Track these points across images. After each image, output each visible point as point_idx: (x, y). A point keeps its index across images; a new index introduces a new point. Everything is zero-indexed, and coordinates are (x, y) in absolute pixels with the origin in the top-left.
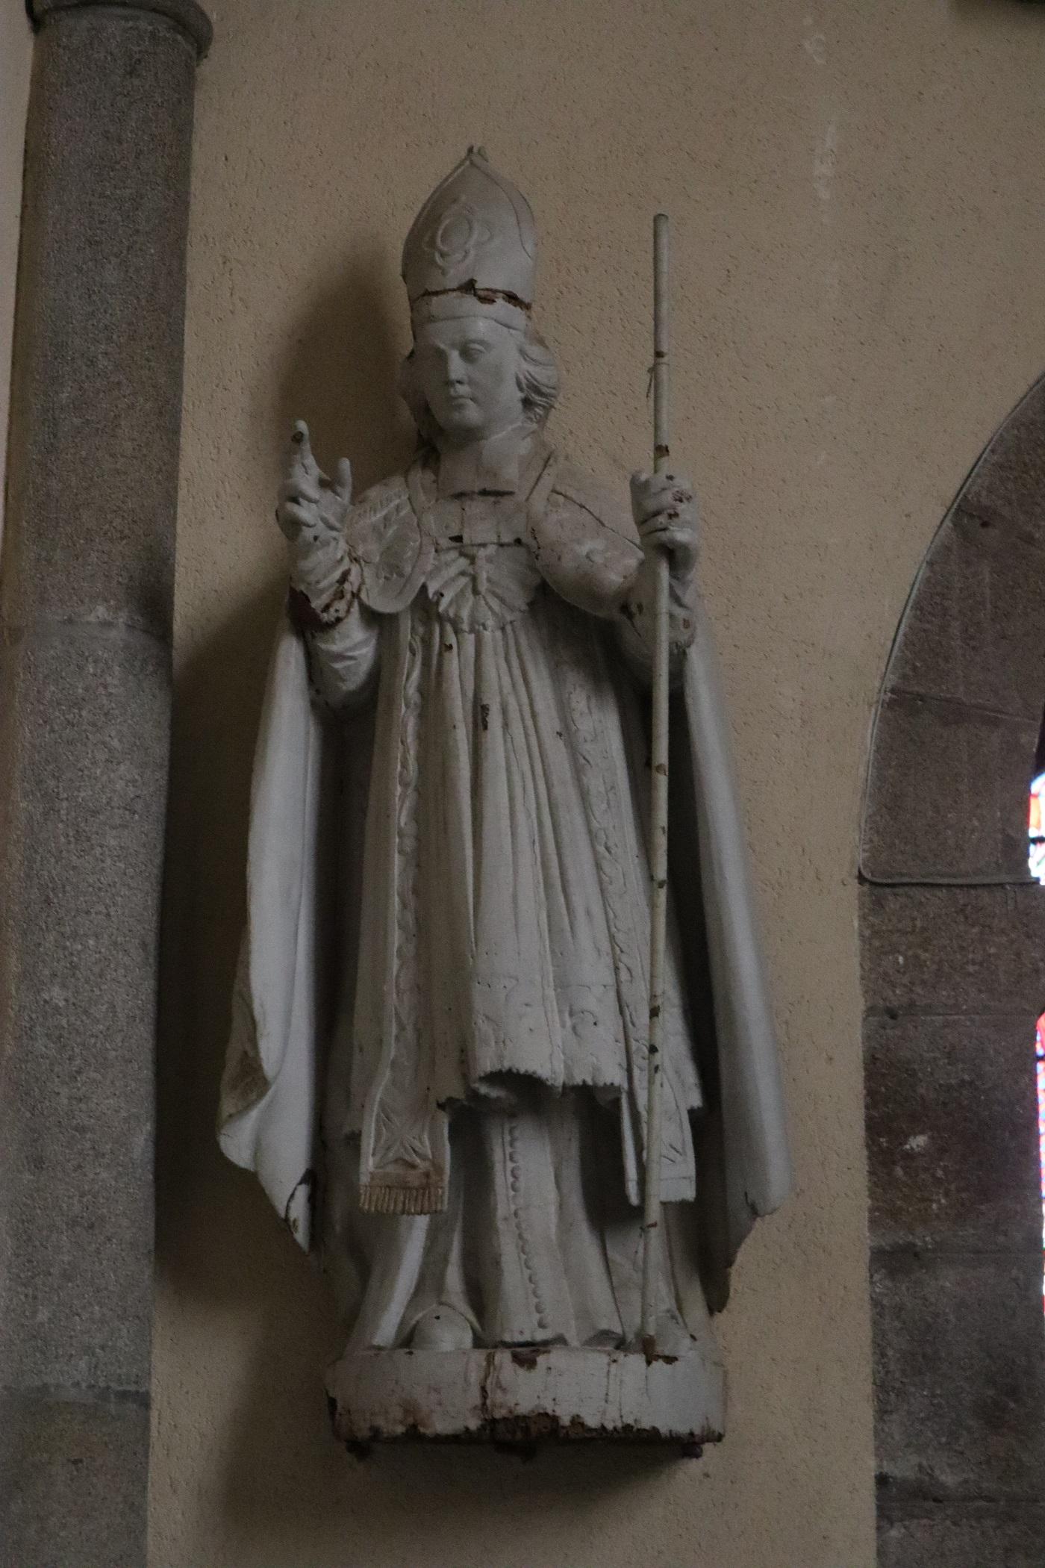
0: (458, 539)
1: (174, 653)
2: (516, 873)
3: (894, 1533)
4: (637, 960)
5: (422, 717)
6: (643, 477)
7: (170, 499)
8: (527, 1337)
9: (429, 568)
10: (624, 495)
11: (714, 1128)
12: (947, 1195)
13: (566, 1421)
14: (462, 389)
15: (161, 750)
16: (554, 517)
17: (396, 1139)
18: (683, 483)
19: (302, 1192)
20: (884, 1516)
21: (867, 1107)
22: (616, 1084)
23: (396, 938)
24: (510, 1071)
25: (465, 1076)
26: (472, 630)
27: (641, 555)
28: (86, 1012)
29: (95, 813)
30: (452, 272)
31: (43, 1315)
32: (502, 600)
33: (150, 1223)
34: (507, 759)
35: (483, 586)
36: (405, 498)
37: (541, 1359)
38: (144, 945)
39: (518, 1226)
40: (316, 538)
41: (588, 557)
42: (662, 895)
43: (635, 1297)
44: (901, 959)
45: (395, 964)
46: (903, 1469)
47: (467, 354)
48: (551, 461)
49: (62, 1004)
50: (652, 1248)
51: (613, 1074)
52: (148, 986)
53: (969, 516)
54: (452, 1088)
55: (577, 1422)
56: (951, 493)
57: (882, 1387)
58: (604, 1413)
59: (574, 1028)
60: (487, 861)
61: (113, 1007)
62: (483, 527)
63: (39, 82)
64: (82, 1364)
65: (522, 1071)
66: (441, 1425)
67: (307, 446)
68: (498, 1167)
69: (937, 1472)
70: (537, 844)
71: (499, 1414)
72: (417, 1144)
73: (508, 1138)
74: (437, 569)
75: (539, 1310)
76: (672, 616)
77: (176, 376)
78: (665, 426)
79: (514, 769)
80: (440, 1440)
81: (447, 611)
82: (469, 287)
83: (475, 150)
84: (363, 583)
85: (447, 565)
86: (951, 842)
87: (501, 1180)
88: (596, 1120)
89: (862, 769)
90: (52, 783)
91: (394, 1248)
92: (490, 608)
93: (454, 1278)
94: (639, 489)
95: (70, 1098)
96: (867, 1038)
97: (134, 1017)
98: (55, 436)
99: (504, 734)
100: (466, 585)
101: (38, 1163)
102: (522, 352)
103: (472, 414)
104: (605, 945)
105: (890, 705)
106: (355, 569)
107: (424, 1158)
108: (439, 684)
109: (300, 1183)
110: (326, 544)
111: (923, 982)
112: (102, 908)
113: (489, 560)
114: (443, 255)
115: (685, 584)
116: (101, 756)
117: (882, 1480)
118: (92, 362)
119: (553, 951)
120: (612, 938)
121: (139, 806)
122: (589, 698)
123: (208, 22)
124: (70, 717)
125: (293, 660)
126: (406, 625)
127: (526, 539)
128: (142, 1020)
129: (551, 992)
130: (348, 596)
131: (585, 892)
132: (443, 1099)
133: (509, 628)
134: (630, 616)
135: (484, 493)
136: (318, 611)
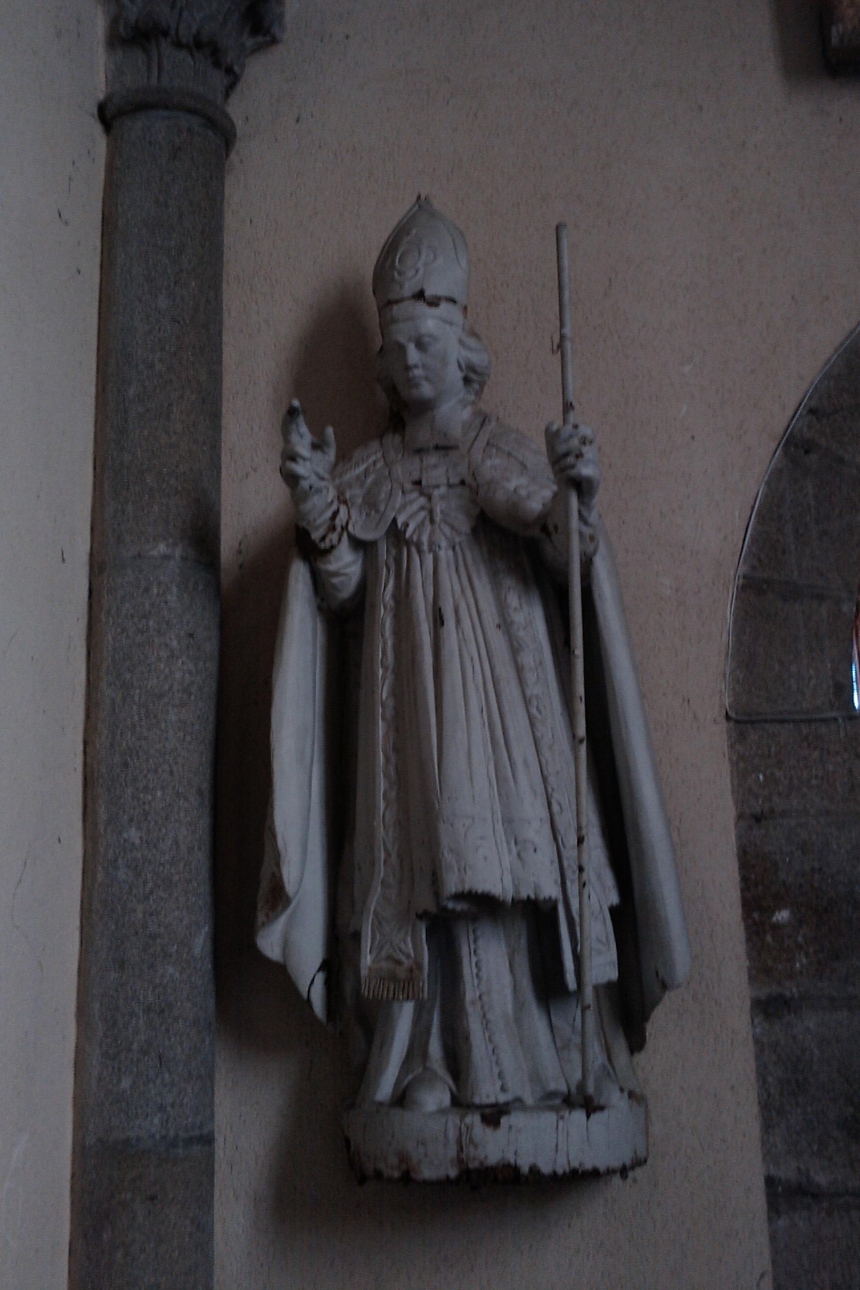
0: (418, 483)
1: (222, 575)
2: (469, 733)
3: (783, 1222)
4: (563, 796)
5: (396, 617)
6: (555, 427)
7: (215, 465)
8: (492, 1100)
9: (397, 506)
10: (541, 443)
11: (631, 920)
12: (807, 955)
13: (525, 1169)
14: (418, 372)
15: (211, 647)
16: (488, 463)
17: (387, 944)
18: (586, 430)
19: (320, 979)
20: (774, 1208)
21: (742, 890)
22: (554, 896)
23: (382, 785)
24: (470, 892)
25: (437, 895)
26: (430, 550)
27: (555, 488)
28: (155, 846)
29: (161, 696)
30: (407, 285)
31: (126, 1083)
32: (452, 527)
33: (211, 1003)
34: (460, 646)
35: (438, 518)
36: (379, 455)
37: (504, 1120)
38: (200, 792)
39: (482, 1007)
40: (311, 488)
41: (515, 490)
42: (583, 749)
43: (576, 1056)
44: (761, 777)
45: (382, 805)
46: (787, 1172)
47: (421, 345)
48: (487, 421)
49: (137, 841)
50: (586, 1020)
51: (550, 890)
52: (204, 824)
53: (796, 447)
54: (427, 903)
55: (534, 1170)
56: (781, 430)
57: (765, 1106)
58: (555, 1161)
59: (519, 855)
60: (447, 726)
61: (176, 842)
62: (438, 472)
63: (110, 168)
64: (156, 1121)
65: (480, 891)
66: (428, 1173)
67: (301, 419)
68: (465, 961)
69: (812, 1173)
70: (485, 712)
71: (473, 1165)
72: (403, 946)
73: (472, 938)
74: (404, 507)
75: (501, 1075)
76: (581, 534)
77: (216, 377)
78: (570, 387)
79: (465, 654)
80: (426, 1183)
81: (411, 536)
82: (420, 295)
83: (423, 197)
84: (349, 517)
85: (411, 502)
86: (794, 687)
87: (468, 970)
88: (539, 924)
89: (725, 635)
90: (128, 676)
91: (389, 1022)
92: (444, 535)
93: (435, 1048)
94: (552, 437)
95: (144, 913)
96: (739, 837)
97: (193, 848)
98: (126, 421)
99: (457, 628)
100: (425, 518)
101: (121, 964)
102: (461, 342)
103: (426, 390)
104: (540, 788)
105: (743, 589)
106: (343, 509)
107: (408, 956)
108: (407, 593)
109: (318, 971)
110: (319, 491)
111: (779, 794)
112: (166, 767)
113: (442, 497)
114: (400, 273)
115: (589, 508)
116: (164, 654)
117: (770, 1181)
118: (151, 366)
119: (500, 794)
120: (545, 779)
121: (193, 689)
122: (520, 598)
123: (233, 125)
124: (140, 626)
125: (300, 578)
126: (383, 548)
127: (469, 480)
128: (200, 849)
129: (499, 827)
130: (339, 529)
131: (523, 747)
132: (420, 912)
133: (458, 548)
134: (549, 534)
135: (437, 448)
136: (317, 541)
